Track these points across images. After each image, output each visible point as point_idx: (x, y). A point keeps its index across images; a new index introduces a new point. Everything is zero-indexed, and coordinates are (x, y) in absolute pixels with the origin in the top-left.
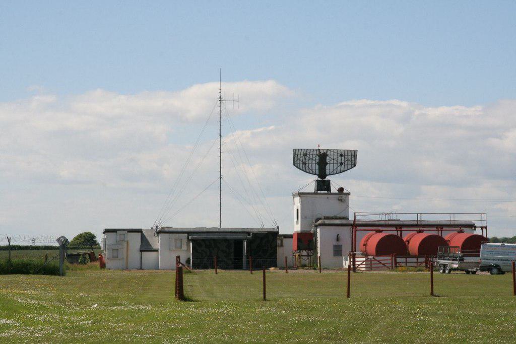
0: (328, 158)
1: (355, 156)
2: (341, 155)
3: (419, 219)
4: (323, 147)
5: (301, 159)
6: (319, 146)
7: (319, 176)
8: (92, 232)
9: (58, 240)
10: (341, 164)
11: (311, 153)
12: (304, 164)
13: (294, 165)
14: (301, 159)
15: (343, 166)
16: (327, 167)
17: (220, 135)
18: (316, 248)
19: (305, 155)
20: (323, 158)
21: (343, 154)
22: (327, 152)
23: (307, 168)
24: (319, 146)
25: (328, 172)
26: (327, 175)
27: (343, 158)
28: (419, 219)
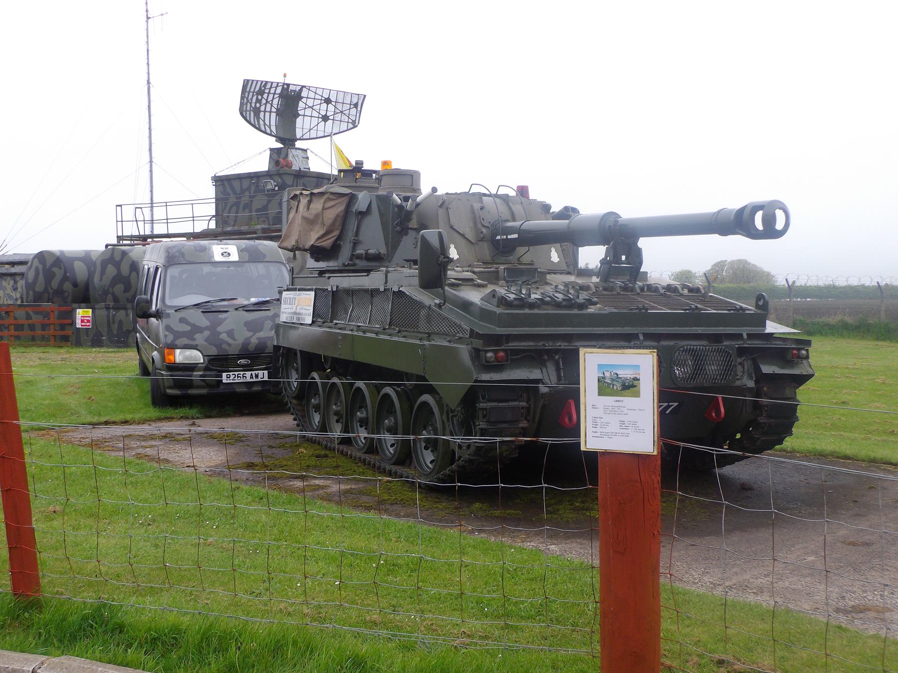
0: (301, 105)
1: (357, 106)
2: (328, 101)
3: (544, 370)
4: (295, 80)
5: (253, 100)
6: (285, 76)
7: (280, 139)
8: (548, 202)
9: (357, 163)
10: (325, 118)
11: (273, 91)
12: (257, 112)
13: (241, 114)
14: (253, 100)
15: (329, 122)
16: (299, 121)
17: (149, 83)
18: (395, 412)
19: (261, 92)
20: (290, 100)
21: (333, 99)
22: (301, 90)
23: (261, 123)
24: (285, 76)
25: (299, 134)
26: (296, 140)
27: (323, 113)
28: (544, 370)
